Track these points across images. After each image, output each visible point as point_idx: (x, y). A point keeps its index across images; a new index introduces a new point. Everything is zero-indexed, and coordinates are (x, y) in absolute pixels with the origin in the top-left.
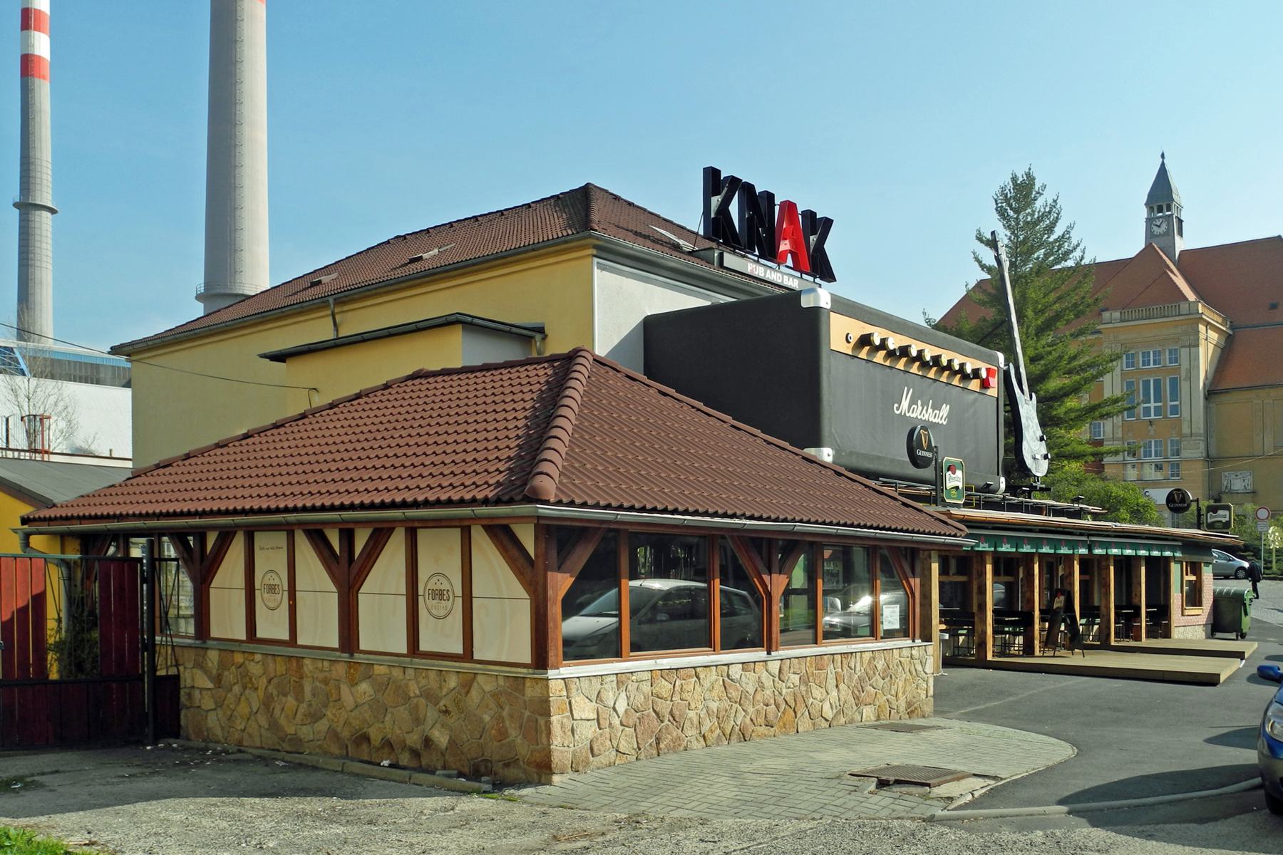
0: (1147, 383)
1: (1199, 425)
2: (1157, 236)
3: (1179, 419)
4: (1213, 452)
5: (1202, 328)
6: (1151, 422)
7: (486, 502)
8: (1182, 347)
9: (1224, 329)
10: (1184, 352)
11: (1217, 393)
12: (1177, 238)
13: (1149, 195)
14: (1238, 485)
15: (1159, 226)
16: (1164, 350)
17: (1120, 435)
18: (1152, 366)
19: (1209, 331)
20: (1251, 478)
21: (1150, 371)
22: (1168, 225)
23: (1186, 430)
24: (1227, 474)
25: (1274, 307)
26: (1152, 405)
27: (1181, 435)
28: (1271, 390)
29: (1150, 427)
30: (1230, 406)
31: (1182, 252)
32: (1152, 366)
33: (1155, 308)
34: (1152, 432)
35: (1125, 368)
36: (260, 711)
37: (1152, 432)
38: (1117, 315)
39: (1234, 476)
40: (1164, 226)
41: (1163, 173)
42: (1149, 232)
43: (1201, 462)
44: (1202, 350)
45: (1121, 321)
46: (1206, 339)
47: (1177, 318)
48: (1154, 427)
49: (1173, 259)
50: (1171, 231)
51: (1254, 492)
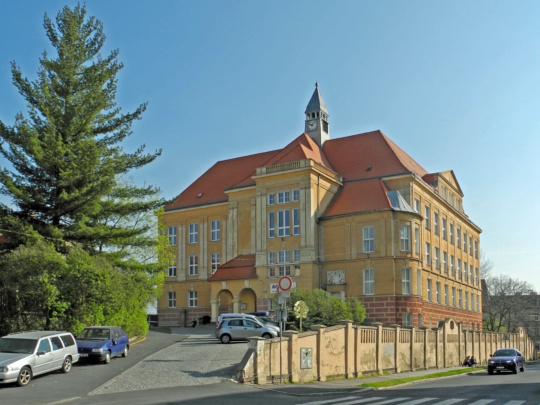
0: (281, 214)
1: (312, 241)
2: (312, 131)
3: (299, 236)
4: (322, 258)
5: (313, 177)
6: (283, 239)
7: (374, 295)
8: (301, 189)
9: (335, 181)
10: (302, 192)
11: (325, 220)
12: (323, 133)
13: (307, 107)
14: (336, 280)
15: (312, 125)
16: (291, 191)
17: (265, 248)
18: (284, 202)
19: (320, 179)
20: (344, 275)
21: (283, 206)
22: (317, 124)
23: (303, 244)
24: (330, 272)
25: (369, 169)
26: (284, 228)
27: (300, 247)
28: (355, 217)
29: (283, 242)
30: (330, 226)
31: (326, 142)
32: (284, 202)
33: (278, 165)
34: (284, 246)
35: (269, 204)
36: (495, 328)
37: (284, 246)
38: (264, 169)
39: (334, 274)
40: (315, 125)
41: (316, 94)
42: (307, 128)
43: (311, 265)
44: (313, 192)
45: (267, 173)
46: (318, 185)
47: (297, 170)
48: (285, 242)
49: (319, 145)
50: (319, 129)
51: (345, 284)
